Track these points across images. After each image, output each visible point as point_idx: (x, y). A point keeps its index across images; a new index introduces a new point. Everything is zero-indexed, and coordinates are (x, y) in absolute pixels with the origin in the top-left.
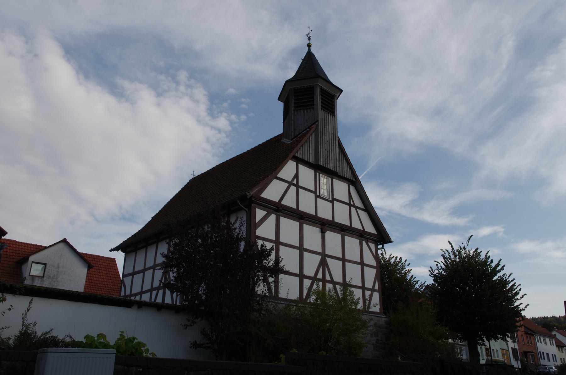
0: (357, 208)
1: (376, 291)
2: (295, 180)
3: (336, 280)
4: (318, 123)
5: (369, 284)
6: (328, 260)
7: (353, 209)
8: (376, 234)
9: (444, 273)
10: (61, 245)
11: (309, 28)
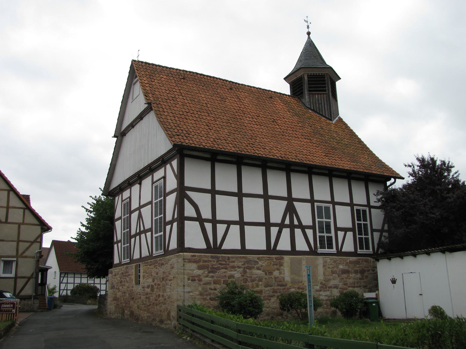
3: (304, 223)
6: (295, 203)
11: (307, 17)
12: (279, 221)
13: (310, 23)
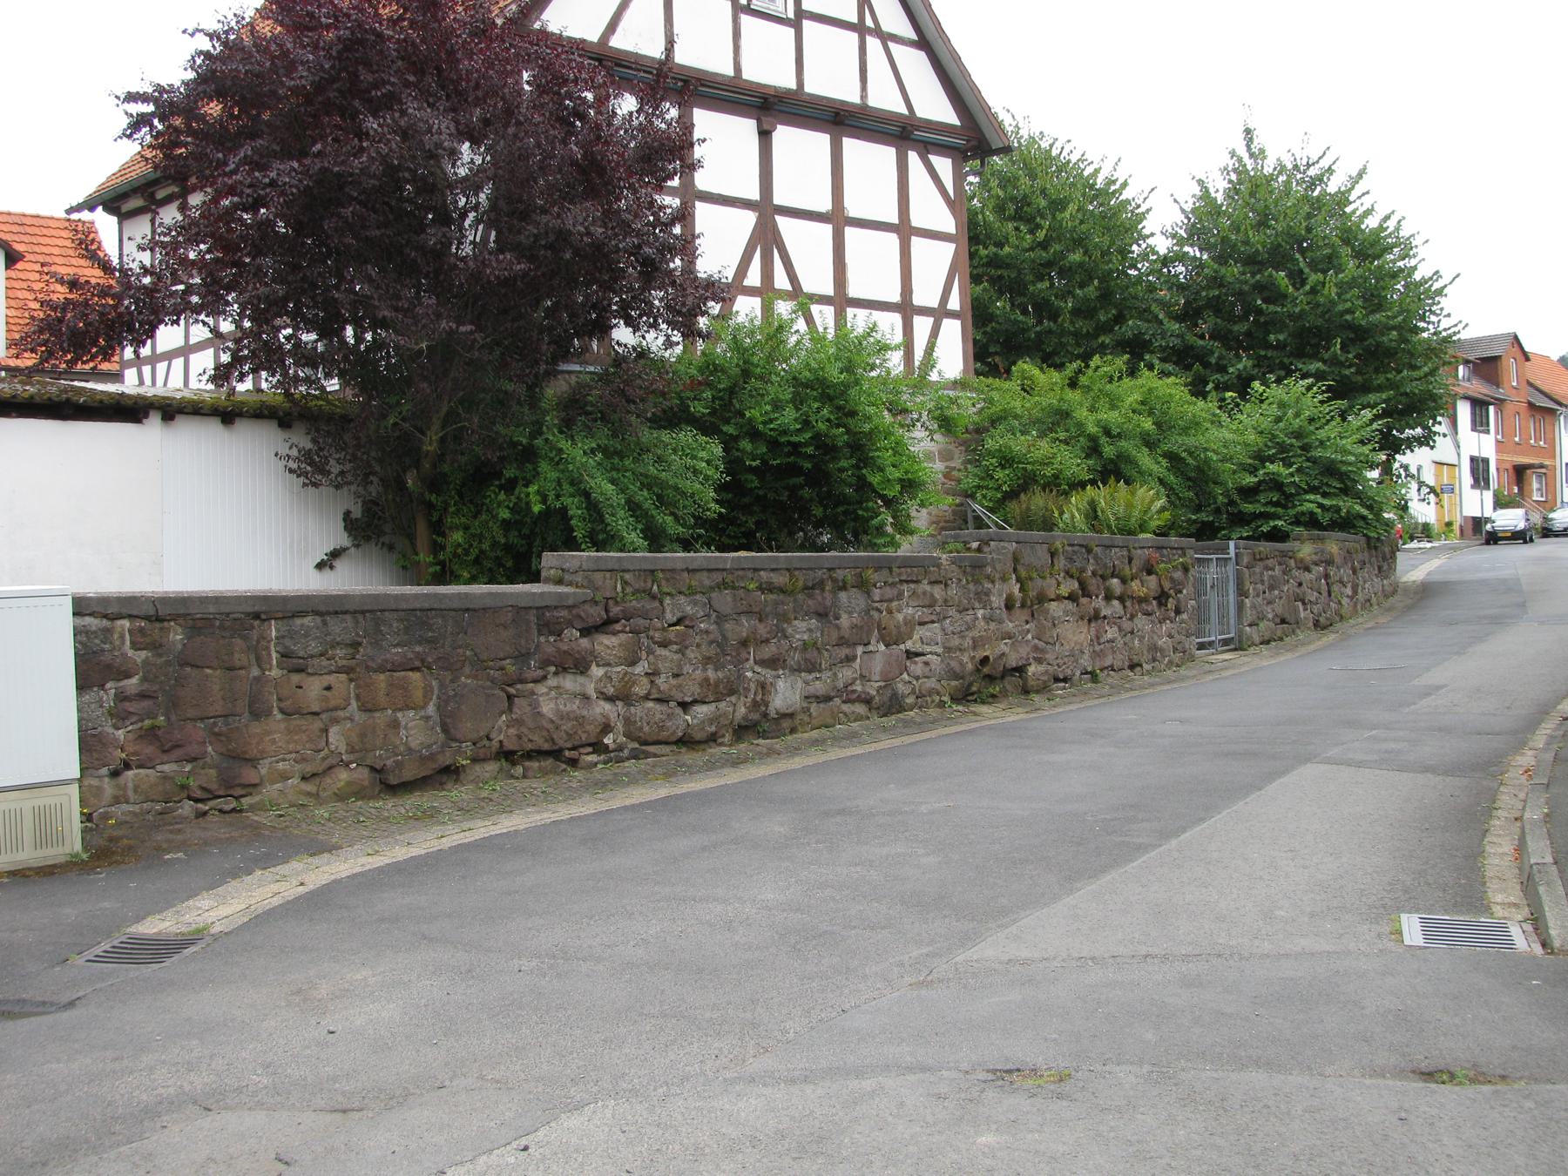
5: (927, 293)
6: (783, 222)
7: (873, 44)
8: (957, 122)
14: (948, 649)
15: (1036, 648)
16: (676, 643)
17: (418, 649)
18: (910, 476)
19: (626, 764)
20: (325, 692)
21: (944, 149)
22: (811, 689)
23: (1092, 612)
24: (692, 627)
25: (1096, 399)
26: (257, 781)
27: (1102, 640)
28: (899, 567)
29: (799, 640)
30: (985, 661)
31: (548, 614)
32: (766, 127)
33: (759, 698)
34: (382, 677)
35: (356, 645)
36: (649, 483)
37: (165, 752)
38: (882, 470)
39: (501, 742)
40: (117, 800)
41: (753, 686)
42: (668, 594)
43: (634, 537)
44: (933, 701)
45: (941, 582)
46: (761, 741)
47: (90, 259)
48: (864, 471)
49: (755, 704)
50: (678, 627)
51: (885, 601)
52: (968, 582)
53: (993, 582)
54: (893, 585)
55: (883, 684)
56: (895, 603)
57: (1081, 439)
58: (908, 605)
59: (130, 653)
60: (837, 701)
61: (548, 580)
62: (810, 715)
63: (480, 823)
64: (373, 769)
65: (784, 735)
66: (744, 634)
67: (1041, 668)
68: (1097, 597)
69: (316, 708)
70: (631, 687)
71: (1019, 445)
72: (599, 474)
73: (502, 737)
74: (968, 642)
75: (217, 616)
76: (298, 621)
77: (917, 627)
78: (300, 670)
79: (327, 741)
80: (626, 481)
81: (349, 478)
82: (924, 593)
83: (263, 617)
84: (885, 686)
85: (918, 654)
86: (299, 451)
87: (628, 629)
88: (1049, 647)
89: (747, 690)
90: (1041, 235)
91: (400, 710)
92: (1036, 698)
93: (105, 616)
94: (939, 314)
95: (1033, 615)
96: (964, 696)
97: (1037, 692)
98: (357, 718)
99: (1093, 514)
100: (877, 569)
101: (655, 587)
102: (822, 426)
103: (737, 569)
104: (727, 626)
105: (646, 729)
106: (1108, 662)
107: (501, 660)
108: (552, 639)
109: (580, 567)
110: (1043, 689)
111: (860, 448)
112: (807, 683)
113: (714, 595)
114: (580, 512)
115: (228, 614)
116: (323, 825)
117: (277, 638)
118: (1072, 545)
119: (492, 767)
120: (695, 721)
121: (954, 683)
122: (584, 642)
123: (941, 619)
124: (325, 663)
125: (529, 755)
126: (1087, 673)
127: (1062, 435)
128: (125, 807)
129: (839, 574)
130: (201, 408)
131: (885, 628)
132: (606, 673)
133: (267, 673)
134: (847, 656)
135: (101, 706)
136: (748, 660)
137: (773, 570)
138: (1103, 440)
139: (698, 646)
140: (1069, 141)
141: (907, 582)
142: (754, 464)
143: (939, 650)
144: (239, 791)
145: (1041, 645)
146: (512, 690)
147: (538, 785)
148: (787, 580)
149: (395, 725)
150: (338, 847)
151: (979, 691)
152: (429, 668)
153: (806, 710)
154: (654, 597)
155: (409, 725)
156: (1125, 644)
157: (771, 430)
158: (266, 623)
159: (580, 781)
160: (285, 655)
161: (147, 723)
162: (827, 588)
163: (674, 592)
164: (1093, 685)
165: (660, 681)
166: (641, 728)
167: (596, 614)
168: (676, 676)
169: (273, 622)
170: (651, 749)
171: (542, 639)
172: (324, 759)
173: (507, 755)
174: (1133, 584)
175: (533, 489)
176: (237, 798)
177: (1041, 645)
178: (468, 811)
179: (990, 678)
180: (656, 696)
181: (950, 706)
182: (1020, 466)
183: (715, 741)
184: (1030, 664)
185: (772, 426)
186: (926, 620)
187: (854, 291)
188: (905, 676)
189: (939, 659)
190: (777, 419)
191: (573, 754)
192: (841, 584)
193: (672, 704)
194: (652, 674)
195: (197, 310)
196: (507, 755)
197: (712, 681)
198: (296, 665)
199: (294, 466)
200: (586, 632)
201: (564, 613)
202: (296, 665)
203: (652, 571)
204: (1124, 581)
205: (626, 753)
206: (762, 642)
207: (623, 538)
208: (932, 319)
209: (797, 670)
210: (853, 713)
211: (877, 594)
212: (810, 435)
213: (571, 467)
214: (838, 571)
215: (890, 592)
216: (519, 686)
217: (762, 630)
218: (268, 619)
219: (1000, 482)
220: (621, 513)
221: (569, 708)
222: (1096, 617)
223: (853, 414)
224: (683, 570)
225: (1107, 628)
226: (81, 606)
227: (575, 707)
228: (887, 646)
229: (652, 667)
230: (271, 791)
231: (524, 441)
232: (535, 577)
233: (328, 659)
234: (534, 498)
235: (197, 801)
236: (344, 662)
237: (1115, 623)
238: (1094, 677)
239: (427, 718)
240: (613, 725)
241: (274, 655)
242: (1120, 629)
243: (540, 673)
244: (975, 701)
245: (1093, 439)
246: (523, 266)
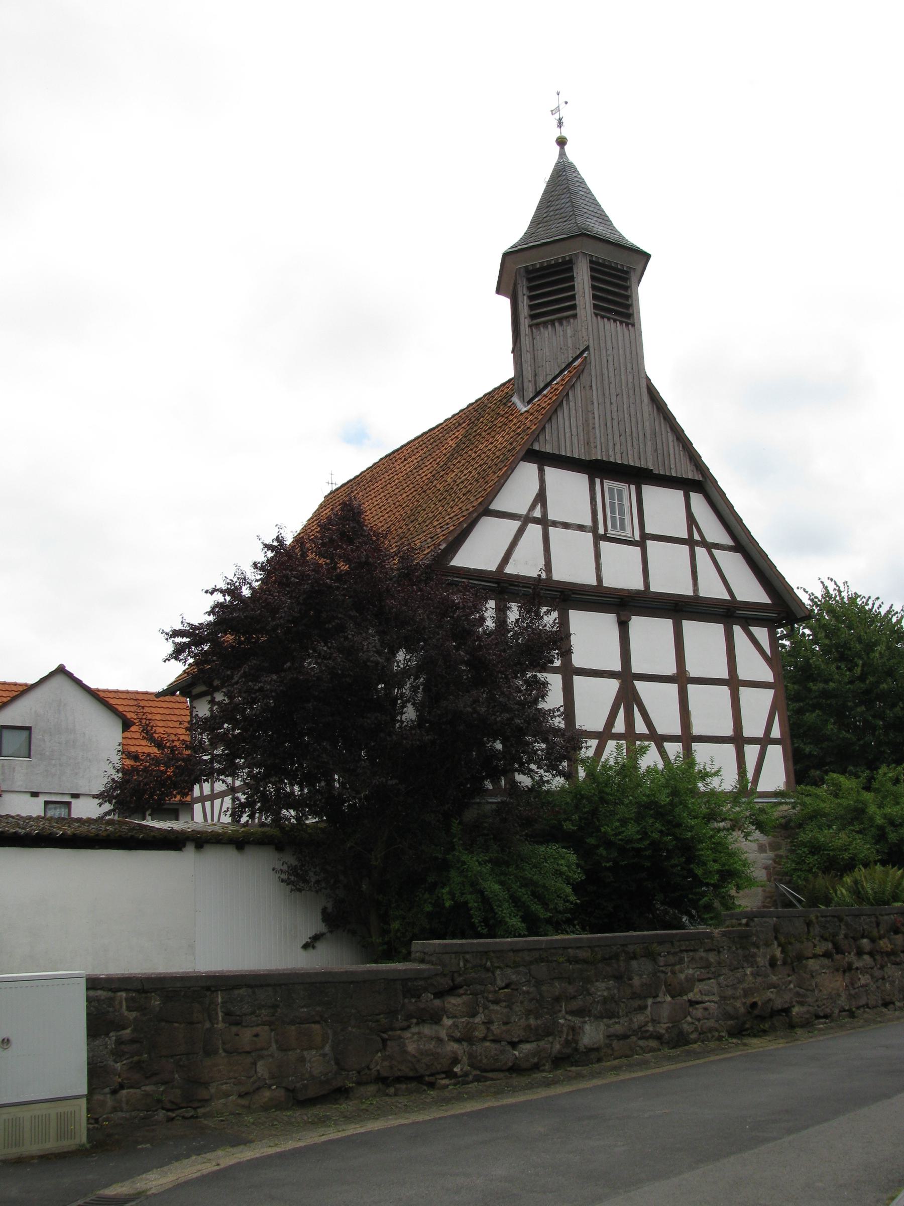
0: (710, 547)
1: (775, 742)
2: (539, 507)
3: (661, 730)
4: (589, 354)
5: (753, 727)
6: (639, 685)
7: (700, 552)
8: (768, 601)
9: (301, 873)
10: (60, 680)
11: (558, 94)
12: (599, 727)
13: (566, 103)
14: (724, 998)
15: (798, 994)
16: (505, 1001)
17: (319, 1009)
18: (727, 867)
19: (470, 1086)
20: (255, 1039)
21: (760, 622)
22: (611, 1030)
23: (846, 965)
24: (517, 990)
25: (884, 797)
26: (207, 1097)
27: (856, 986)
28: (679, 941)
29: (600, 996)
30: (754, 1005)
31: (410, 984)
32: (623, 619)
33: (570, 1038)
34: (293, 1028)
35: (275, 1007)
36: (527, 883)
37: (147, 1078)
38: (704, 864)
39: (378, 1071)
40: (115, 1110)
41: (565, 1029)
42: (498, 967)
43: (515, 922)
44: (713, 1036)
45: (714, 950)
46: (573, 1068)
47: (149, 740)
48: (692, 866)
49: (567, 1043)
50: (506, 990)
51: (669, 965)
52: (737, 949)
53: (758, 947)
54: (675, 954)
55: (670, 1025)
56: (677, 967)
57: (872, 829)
58: (688, 967)
59: (126, 1013)
60: (634, 1038)
61: (414, 960)
62: (612, 1049)
63: (353, 1126)
64: (287, 1090)
65: (592, 1064)
66: (557, 993)
67: (804, 1009)
68: (849, 953)
69: (248, 1048)
70: (472, 1032)
71: (823, 836)
72: (490, 878)
73: (378, 1067)
74: (739, 992)
75: (182, 989)
76: (236, 992)
77: (697, 983)
78: (237, 1024)
79: (256, 1071)
80: (510, 882)
81: (323, 885)
82: (701, 958)
83: (213, 989)
84: (672, 1027)
85: (698, 1003)
86: (289, 867)
87: (469, 992)
88: (809, 993)
89: (561, 1032)
90: (858, 671)
91: (306, 1049)
92: (799, 1031)
93: (110, 990)
94: (765, 742)
95: (793, 970)
96: (740, 1031)
97: (802, 1026)
98: (276, 1055)
99: (857, 893)
100: (660, 943)
101: (489, 963)
102: (656, 835)
103: (550, 949)
104: (544, 988)
105: (485, 1061)
106: (863, 1001)
107: (377, 1015)
108: (413, 1000)
109: (434, 951)
110: (806, 1025)
111: (688, 849)
112: (608, 1026)
113: (532, 967)
114: (476, 904)
115: (189, 988)
116: (249, 1127)
117: (222, 1003)
118: (826, 917)
119: (372, 1088)
120: (521, 1055)
121: (730, 1023)
122: (437, 1002)
123: (717, 976)
124: (254, 1019)
125: (399, 1080)
126: (845, 1011)
127: (857, 828)
128: (120, 1114)
129: (631, 948)
130: (221, 839)
131: (670, 985)
132: (454, 1023)
133: (215, 1026)
134: (639, 1006)
135: (106, 1048)
136: (560, 1011)
137: (578, 948)
138: (889, 829)
139: (522, 1002)
140: (878, 598)
141: (687, 951)
142: (608, 865)
143: (716, 999)
144: (196, 1104)
145: (802, 991)
146: (385, 1036)
147: (403, 1100)
148: (589, 954)
149: (302, 1060)
150: (252, 1141)
151: (752, 1028)
152: (326, 1021)
153: (609, 1046)
154: (487, 970)
155: (312, 1060)
156: (878, 987)
157: (620, 840)
158: (215, 993)
159: (433, 1098)
160: (228, 1014)
161: (136, 1059)
162: (622, 958)
163: (502, 965)
164: (850, 1020)
165: (494, 1027)
166: (481, 1061)
167: (446, 983)
168: (506, 1023)
169: (219, 992)
170: (490, 1075)
171: (406, 1001)
172: (254, 1083)
173: (382, 1080)
174: (881, 942)
175: (446, 890)
176: (195, 1109)
177: (802, 991)
178: (350, 1118)
179: (762, 1018)
180: (491, 1038)
181: (726, 1040)
182: (825, 852)
183: (538, 1068)
184: (794, 1006)
185: (620, 837)
186: (704, 977)
187: (697, 729)
188: (689, 1019)
189: (716, 1005)
190: (623, 832)
191: (432, 1079)
192: (632, 955)
193: (503, 1043)
194: (488, 1023)
195: (221, 772)
196: (382, 1080)
197: (533, 1026)
198: (234, 1020)
199: (284, 876)
200: (439, 995)
201: (421, 983)
202: (234, 1020)
203: (486, 952)
204: (873, 940)
205: (471, 1077)
206: (571, 998)
207: (506, 923)
208: (759, 747)
209: (600, 1017)
210: (648, 1046)
211: (661, 961)
212: (648, 842)
213: (469, 874)
214: (629, 946)
215: (672, 959)
216: (390, 1033)
217: (571, 990)
218: (217, 991)
219: (811, 865)
220: (506, 905)
221: (427, 1047)
222: (849, 968)
223: (679, 825)
224: (510, 951)
225: (860, 976)
226: (93, 983)
227: (432, 1046)
228: (673, 997)
229: (487, 1018)
230: (217, 1104)
231: (440, 856)
232: (407, 958)
233: (256, 1016)
234: (445, 897)
235: (168, 1110)
236: (267, 1018)
237: (867, 973)
238: (852, 1015)
239: (324, 1055)
240: (460, 1058)
241: (220, 1014)
242: (872, 976)
243: (405, 1024)
244: (749, 1035)
245: (881, 828)
246: (430, 737)
